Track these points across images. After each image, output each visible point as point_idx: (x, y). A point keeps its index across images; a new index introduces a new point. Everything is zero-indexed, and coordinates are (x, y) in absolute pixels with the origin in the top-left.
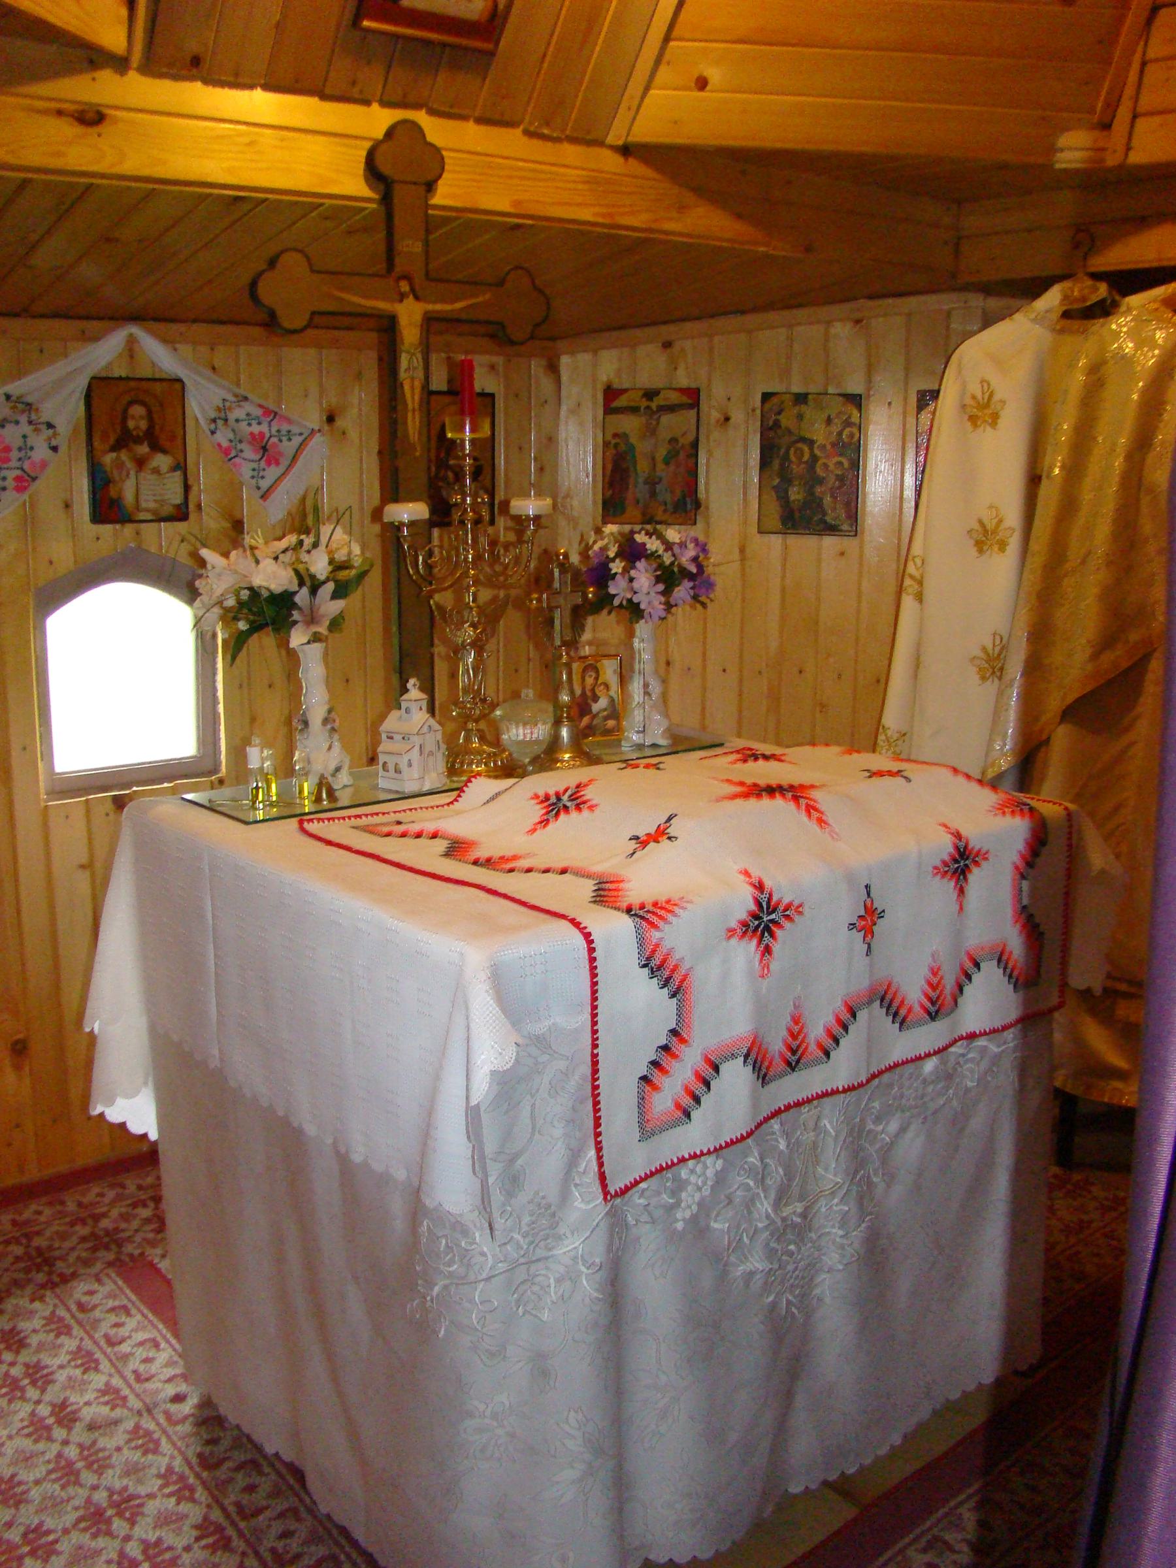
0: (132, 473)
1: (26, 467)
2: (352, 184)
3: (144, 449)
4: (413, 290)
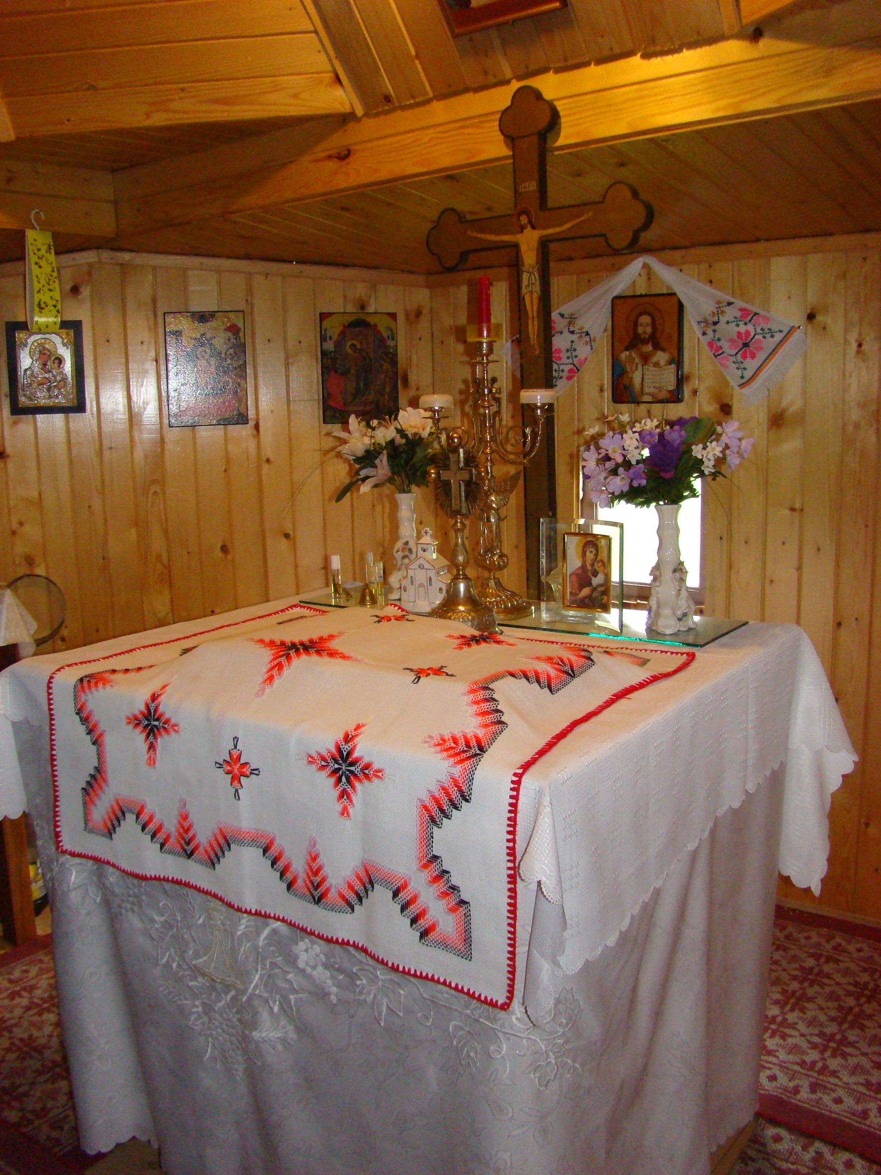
0: (640, 366)
1: (575, 363)
2: (496, 148)
3: (649, 348)
4: (530, 222)
